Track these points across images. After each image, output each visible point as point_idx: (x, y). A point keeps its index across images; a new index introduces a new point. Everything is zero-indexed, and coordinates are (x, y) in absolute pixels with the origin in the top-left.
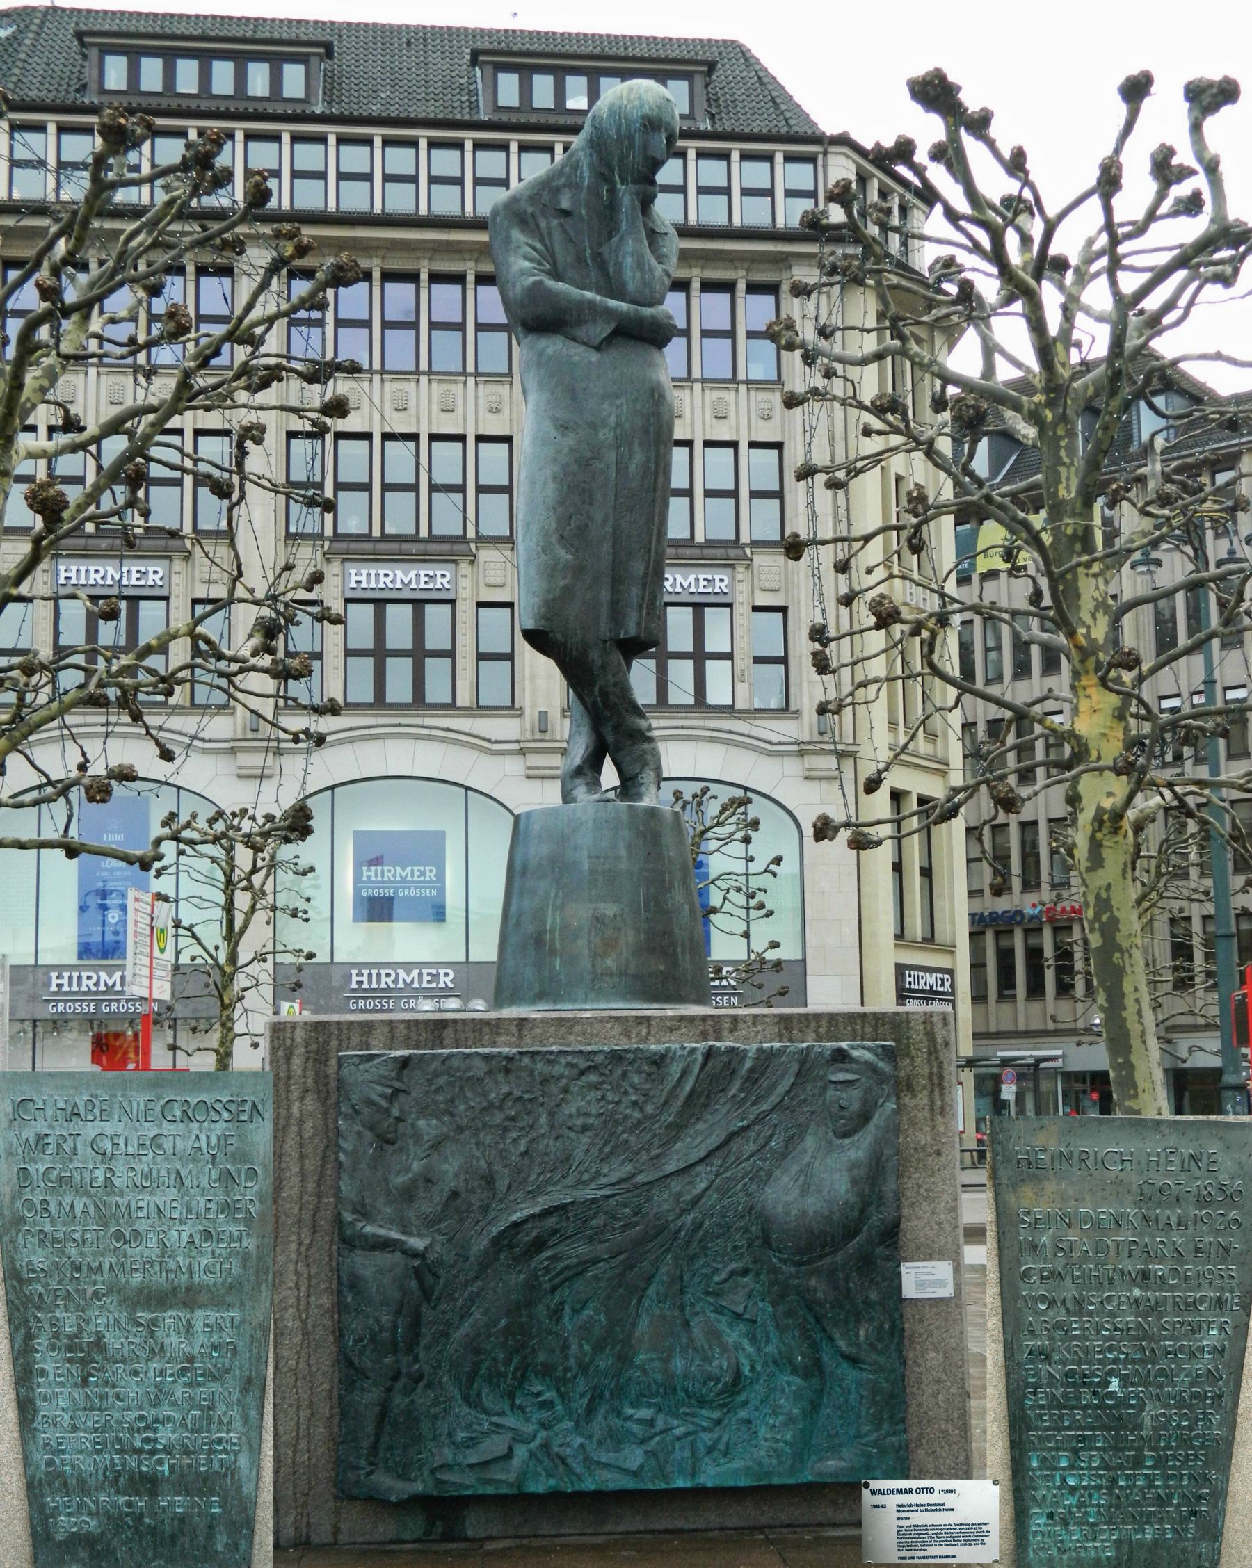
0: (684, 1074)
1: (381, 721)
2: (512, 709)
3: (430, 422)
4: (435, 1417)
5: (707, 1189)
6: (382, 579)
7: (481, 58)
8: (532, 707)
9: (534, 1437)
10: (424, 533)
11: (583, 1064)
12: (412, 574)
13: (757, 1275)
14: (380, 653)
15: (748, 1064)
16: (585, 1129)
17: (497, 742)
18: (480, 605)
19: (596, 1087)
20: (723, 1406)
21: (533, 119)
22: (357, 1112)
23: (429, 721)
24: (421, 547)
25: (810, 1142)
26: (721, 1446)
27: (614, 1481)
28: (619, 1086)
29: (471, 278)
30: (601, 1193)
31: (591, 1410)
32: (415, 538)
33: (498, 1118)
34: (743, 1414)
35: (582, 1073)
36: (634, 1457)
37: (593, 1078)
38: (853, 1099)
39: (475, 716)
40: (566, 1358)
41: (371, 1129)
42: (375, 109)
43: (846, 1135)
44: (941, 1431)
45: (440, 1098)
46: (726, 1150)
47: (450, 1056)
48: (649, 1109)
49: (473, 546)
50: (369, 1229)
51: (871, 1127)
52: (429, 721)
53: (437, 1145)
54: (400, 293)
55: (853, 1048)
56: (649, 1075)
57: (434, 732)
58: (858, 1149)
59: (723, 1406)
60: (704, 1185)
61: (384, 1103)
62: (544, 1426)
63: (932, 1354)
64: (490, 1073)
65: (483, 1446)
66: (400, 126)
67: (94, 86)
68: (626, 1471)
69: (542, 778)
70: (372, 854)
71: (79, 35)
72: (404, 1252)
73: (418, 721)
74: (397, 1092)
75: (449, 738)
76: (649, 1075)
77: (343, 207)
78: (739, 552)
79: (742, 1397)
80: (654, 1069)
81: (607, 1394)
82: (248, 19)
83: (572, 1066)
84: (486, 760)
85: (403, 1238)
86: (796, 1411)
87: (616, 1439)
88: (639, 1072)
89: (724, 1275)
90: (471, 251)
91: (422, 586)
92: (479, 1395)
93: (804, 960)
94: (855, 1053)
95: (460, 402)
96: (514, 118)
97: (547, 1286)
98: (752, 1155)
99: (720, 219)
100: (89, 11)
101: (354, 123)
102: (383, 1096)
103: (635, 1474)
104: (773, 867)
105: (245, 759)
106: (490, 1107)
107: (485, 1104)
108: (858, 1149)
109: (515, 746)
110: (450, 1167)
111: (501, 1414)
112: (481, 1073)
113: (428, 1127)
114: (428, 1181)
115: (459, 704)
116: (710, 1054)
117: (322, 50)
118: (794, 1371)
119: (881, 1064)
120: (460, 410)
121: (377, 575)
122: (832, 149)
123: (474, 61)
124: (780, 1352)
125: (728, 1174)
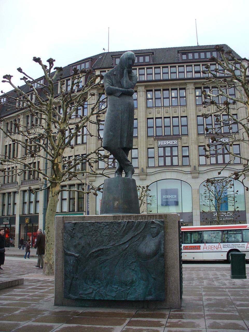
0: (124, 226)
1: (165, 169)
2: (189, 166)
3: (172, 115)
4: (80, 285)
5: (128, 247)
6: (164, 143)
7: (179, 52)
8: (193, 165)
9: (97, 290)
10: (172, 134)
11: (106, 224)
12: (170, 142)
13: (137, 262)
14: (172, 156)
15: (136, 224)
16: (106, 236)
17: (186, 172)
18: (183, 147)
19: (107, 228)
20: (130, 286)
21: (195, 61)
22: (67, 232)
23: (174, 168)
24: (171, 137)
25: (147, 238)
26: (130, 293)
27: (110, 298)
28: (112, 228)
29: (178, 89)
30: (109, 247)
31: (107, 286)
32: (170, 135)
33: (91, 234)
34: (134, 287)
35: (106, 226)
36: (114, 294)
37: (108, 227)
38: (155, 230)
39: (182, 167)
40: (102, 276)
41: (70, 235)
42: (161, 62)
43: (153, 237)
44: (173, 292)
45: (81, 230)
46: (131, 240)
47: (83, 222)
48: (118, 232)
49: (181, 136)
50: (69, 252)
51: (159, 236)
52: (174, 168)
53: (80, 238)
54: (166, 93)
55: (155, 221)
56: (118, 226)
57: (175, 170)
58: (157, 239)
59: (130, 286)
60: (127, 246)
61: (72, 231)
62: (99, 288)
63: (172, 278)
64: (90, 225)
65: (88, 291)
66: (165, 65)
67: (114, 64)
68: (112, 297)
69: (195, 178)
70: (166, 192)
71: (112, 56)
72: (74, 256)
73: (172, 168)
74: (74, 229)
75: (178, 172)
76: (118, 226)
77: (156, 79)
78: (230, 134)
79: (134, 284)
80: (118, 225)
81: (109, 283)
82: (140, 50)
83: (104, 224)
84: (184, 175)
85: (74, 254)
86: (144, 287)
87: (112, 291)
88: (116, 225)
89: (131, 262)
90: (170, 85)
91: (172, 144)
92: (87, 282)
93: (246, 211)
94: (156, 222)
95: (177, 111)
96: (192, 61)
97: (99, 263)
98: (136, 241)
99: (175, 78)
100: (114, 52)
101: (157, 64)
102: (71, 229)
103: (114, 297)
104: (237, 193)
105: (141, 177)
106: (89, 232)
107: (89, 231)
108: (157, 239)
109: (190, 172)
110: (83, 242)
111: (91, 285)
112: (88, 226)
113: (79, 235)
114: (79, 244)
115: (179, 165)
116: (128, 222)
117: (152, 54)
118: (143, 280)
119: (161, 224)
120: (177, 112)
121: (164, 142)
122: (243, 61)
123: (178, 53)
124: (141, 276)
125: (132, 244)
